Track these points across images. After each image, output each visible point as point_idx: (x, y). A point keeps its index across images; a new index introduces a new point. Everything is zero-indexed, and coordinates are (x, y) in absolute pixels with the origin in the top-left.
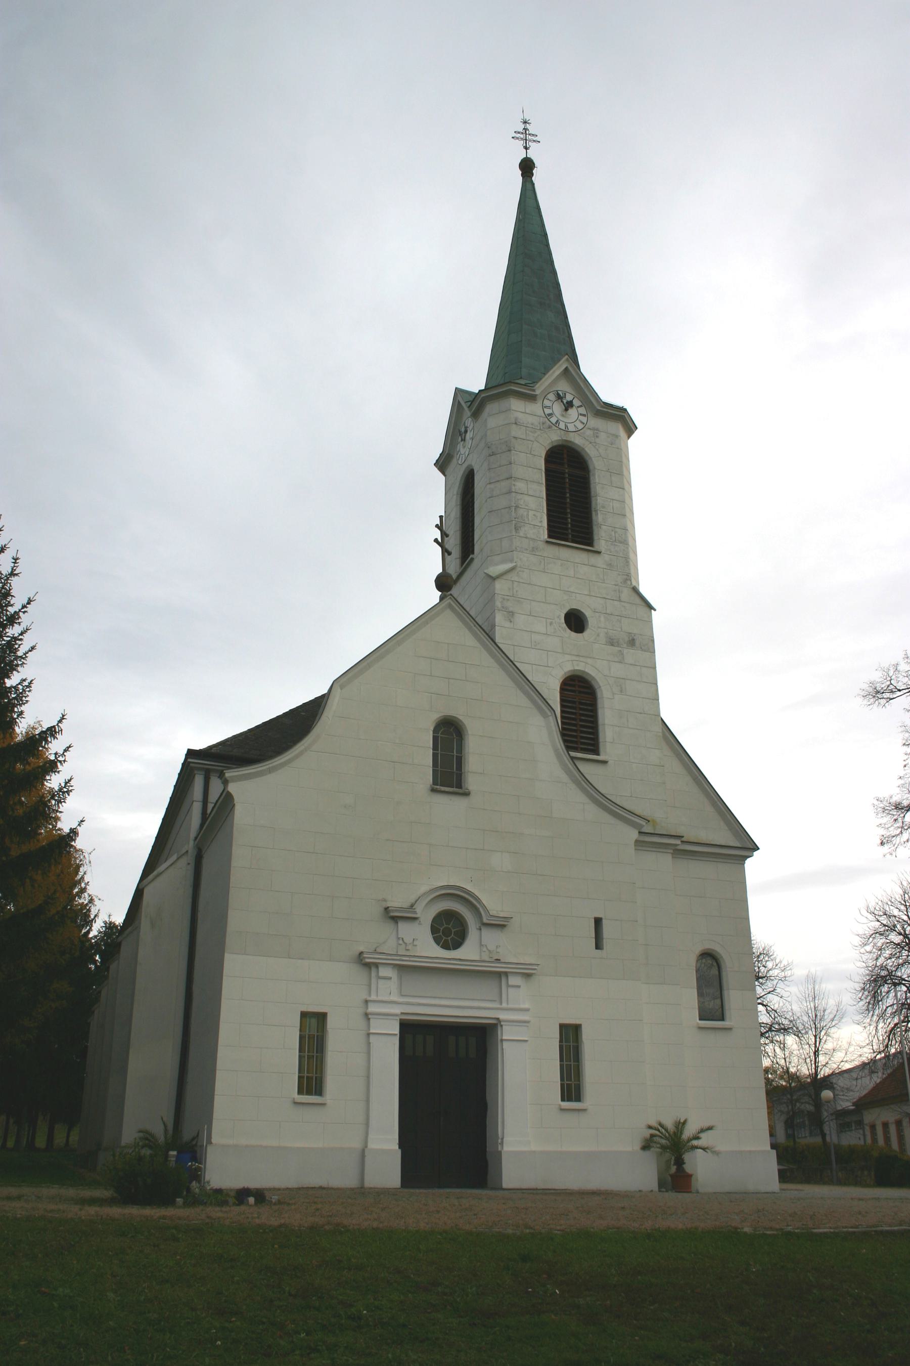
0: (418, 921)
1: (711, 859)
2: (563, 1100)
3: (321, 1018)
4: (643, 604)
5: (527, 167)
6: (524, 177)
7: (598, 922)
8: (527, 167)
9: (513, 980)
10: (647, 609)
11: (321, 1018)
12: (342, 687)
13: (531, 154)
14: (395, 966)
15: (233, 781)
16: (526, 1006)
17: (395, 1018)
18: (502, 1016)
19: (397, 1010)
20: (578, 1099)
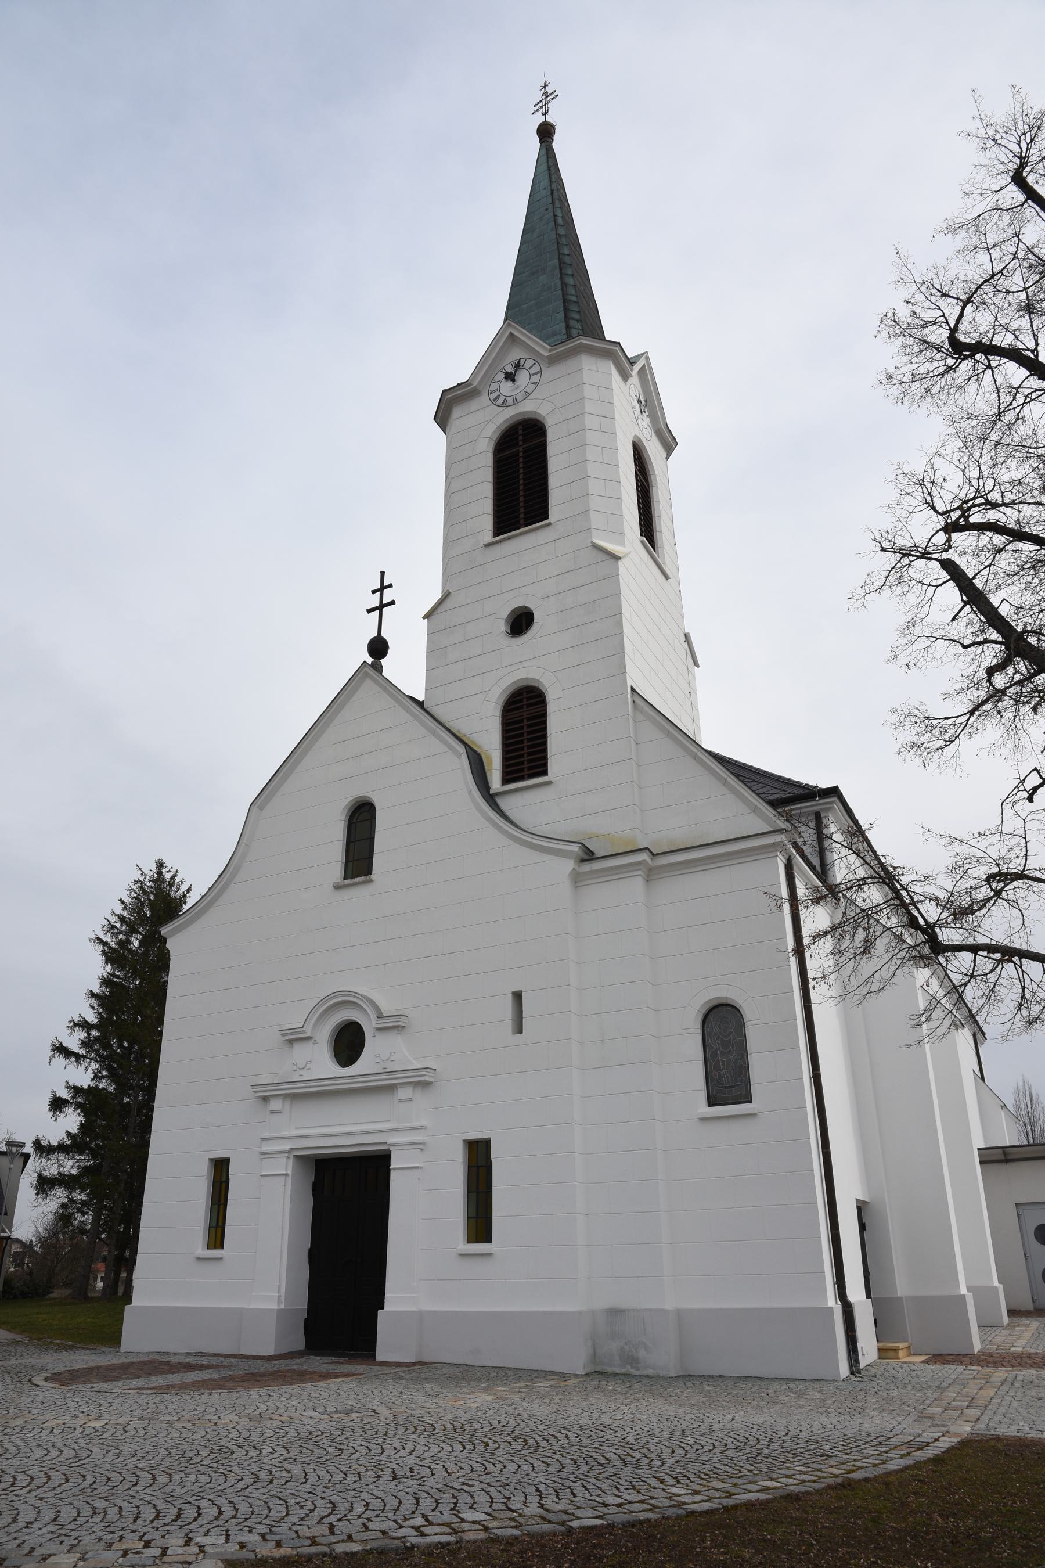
0: (313, 1041)
1: (753, 858)
2: (469, 1241)
3: (487, 1143)
4: (606, 557)
5: (546, 132)
6: (544, 142)
7: (518, 996)
8: (546, 132)
9: (403, 1093)
10: (612, 561)
11: (487, 1143)
12: (261, 808)
13: (549, 119)
14: (286, 1096)
15: (170, 937)
16: (423, 1122)
17: (282, 1155)
18: (392, 1139)
19: (287, 1146)
20: (488, 1239)
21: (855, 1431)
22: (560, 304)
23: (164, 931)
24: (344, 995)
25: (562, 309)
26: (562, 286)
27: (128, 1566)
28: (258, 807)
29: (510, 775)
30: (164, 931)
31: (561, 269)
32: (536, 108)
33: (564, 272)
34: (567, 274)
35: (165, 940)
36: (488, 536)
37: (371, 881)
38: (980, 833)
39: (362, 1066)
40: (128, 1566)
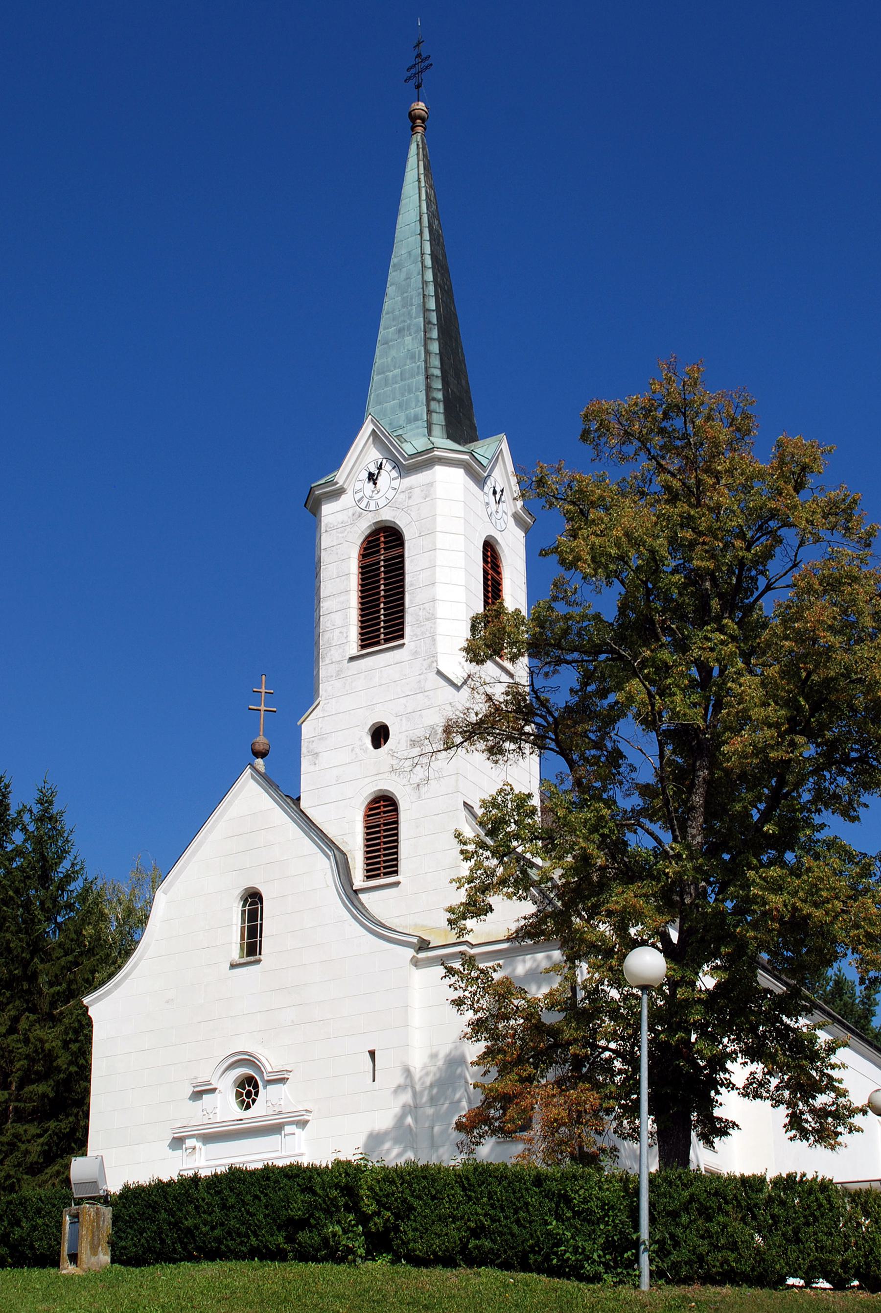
15: (91, 1005)
21: (42, 1006)
22: (421, 378)
23: (86, 1001)
24: (242, 1054)
25: (424, 388)
26: (425, 356)
27: (784, 587)
28: (163, 892)
29: (372, 872)
30: (86, 1001)
31: (425, 332)
32: (409, 74)
33: (428, 336)
34: (431, 339)
35: (87, 1008)
36: (353, 648)
37: (258, 961)
38: (489, 1072)
39: (255, 1110)
40: (784, 587)
